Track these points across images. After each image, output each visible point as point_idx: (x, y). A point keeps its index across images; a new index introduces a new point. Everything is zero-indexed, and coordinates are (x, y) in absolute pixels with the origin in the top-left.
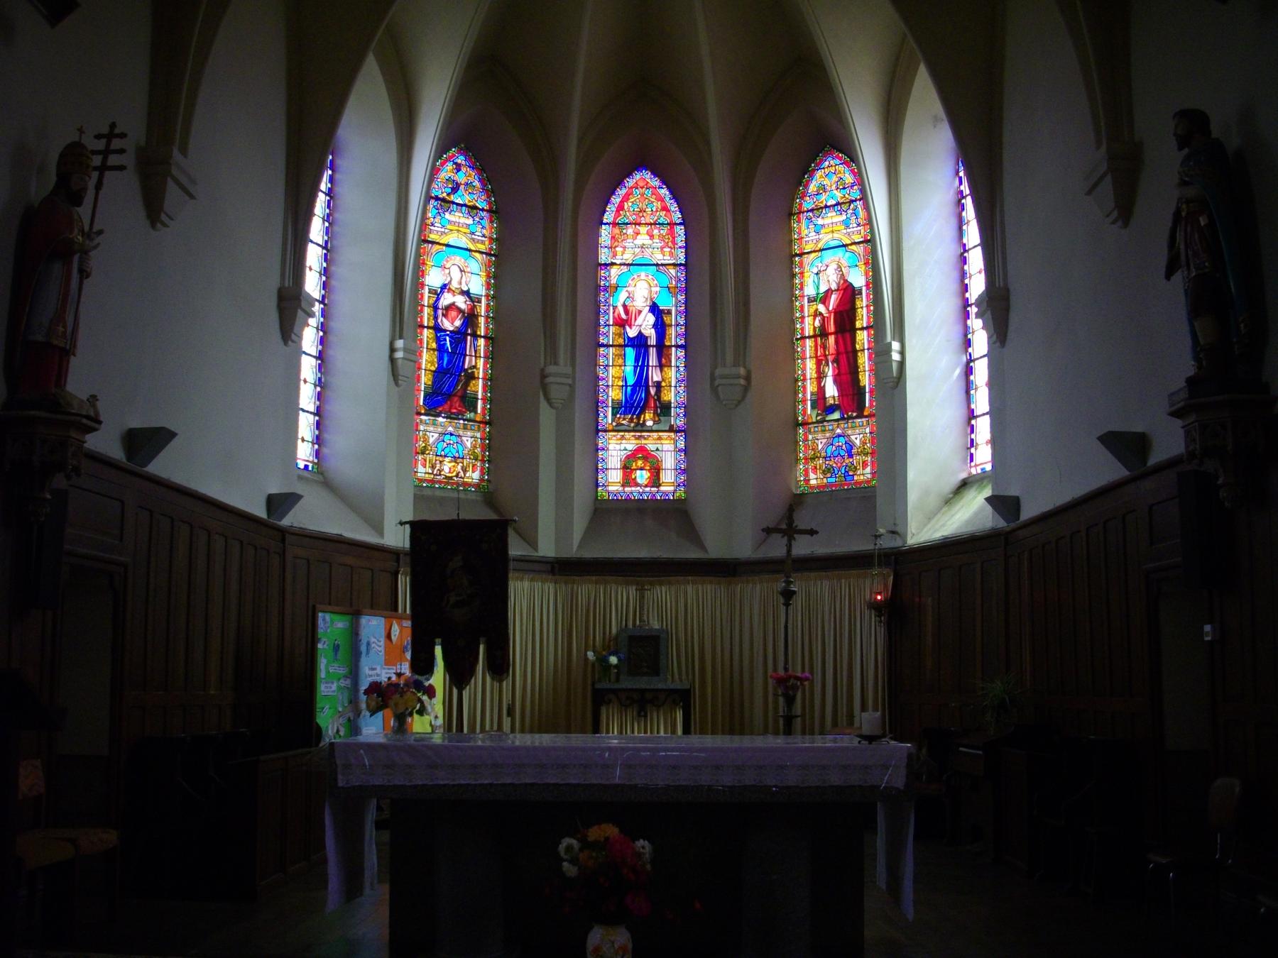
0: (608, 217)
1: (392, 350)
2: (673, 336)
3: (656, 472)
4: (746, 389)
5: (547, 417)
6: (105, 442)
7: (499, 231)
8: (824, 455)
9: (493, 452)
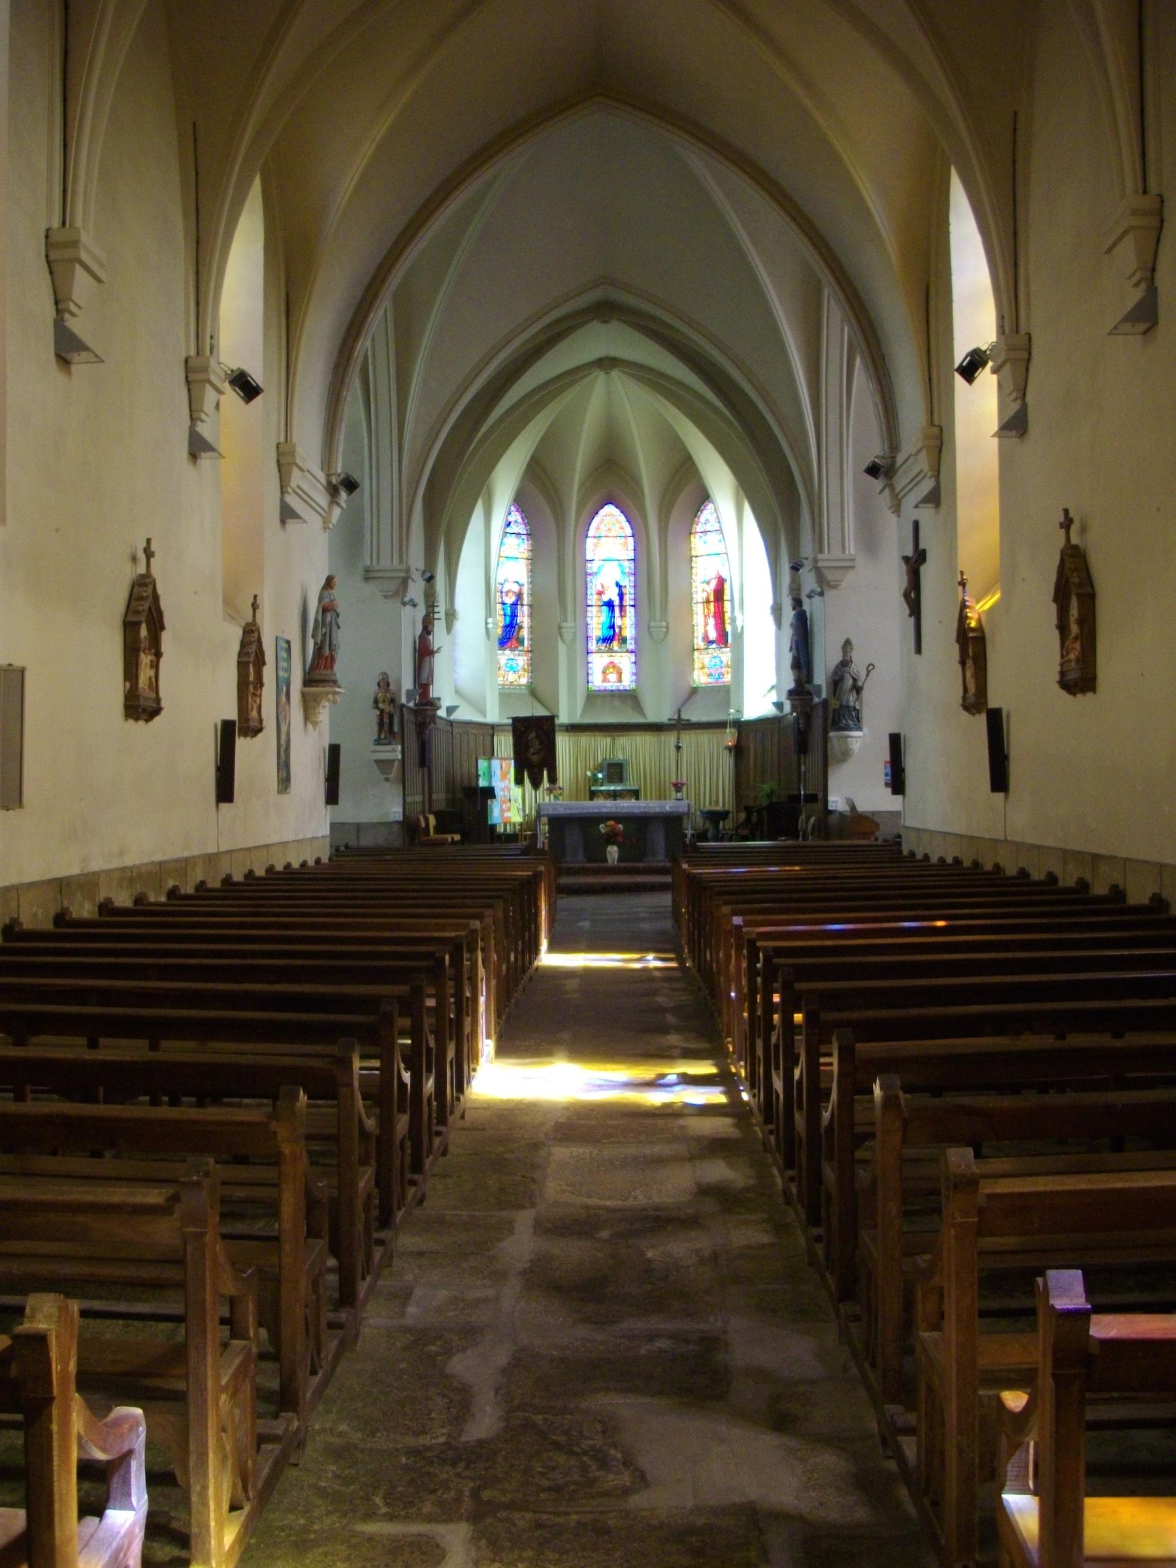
0: (591, 533)
1: (487, 623)
2: (628, 600)
3: (620, 674)
4: (667, 633)
5: (562, 649)
6: (442, 713)
7: (532, 545)
8: (707, 668)
9: (534, 667)
